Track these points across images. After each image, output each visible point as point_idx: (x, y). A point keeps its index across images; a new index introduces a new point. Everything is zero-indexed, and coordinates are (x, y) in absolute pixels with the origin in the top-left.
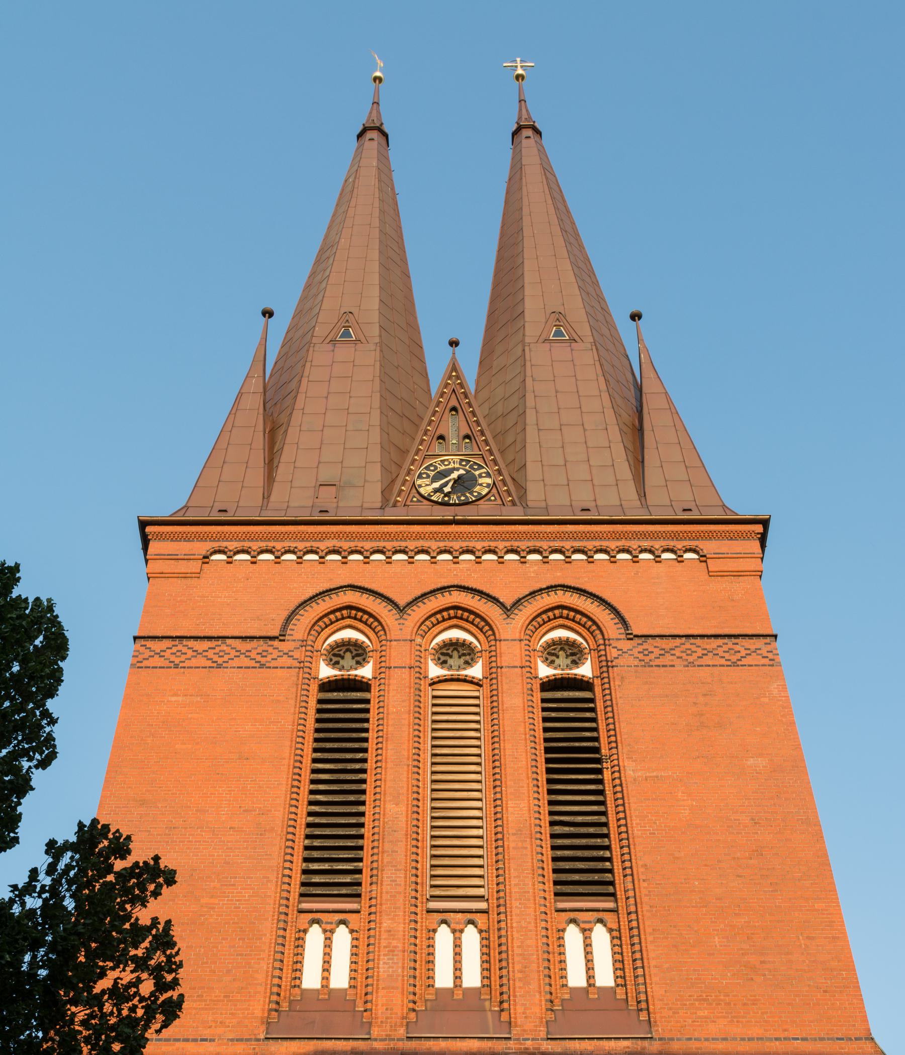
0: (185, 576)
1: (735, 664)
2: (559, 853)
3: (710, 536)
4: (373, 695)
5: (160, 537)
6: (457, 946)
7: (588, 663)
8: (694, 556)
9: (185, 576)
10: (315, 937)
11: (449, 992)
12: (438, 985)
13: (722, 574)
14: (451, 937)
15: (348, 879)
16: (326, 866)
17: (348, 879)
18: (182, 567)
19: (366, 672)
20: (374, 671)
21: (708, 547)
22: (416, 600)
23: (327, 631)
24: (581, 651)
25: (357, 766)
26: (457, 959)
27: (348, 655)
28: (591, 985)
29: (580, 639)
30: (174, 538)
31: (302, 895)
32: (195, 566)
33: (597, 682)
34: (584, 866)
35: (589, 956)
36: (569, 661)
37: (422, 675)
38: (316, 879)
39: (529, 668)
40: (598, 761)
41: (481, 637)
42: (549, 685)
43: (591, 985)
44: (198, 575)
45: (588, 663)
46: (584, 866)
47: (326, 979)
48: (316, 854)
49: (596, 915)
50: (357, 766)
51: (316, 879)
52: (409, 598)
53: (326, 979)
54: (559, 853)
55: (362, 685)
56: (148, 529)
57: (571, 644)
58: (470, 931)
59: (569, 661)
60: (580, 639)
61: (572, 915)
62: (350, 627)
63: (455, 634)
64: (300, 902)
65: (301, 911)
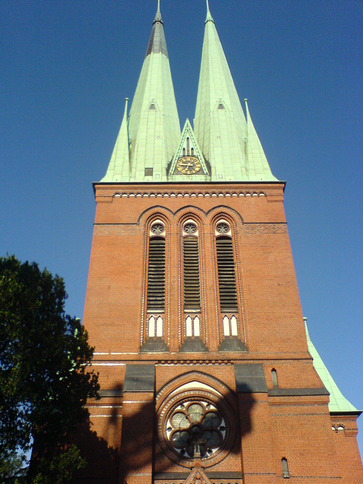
0: (107, 202)
1: (274, 233)
2: (222, 294)
3: (269, 188)
4: (233, 241)
5: (99, 188)
6: (193, 323)
7: (198, 232)
8: (263, 195)
9: (107, 202)
10: (226, 321)
11: (189, 337)
12: (195, 335)
13: (272, 201)
14: (228, 320)
15: (160, 303)
16: (154, 299)
17: (160, 303)
18: (107, 199)
19: (164, 234)
20: (166, 234)
21: (268, 192)
22: (178, 211)
23: (152, 221)
24: (195, 226)
25: (162, 266)
26: (193, 327)
27: (223, 227)
28: (156, 336)
29: (162, 222)
30: (103, 188)
31: (148, 308)
32: (110, 199)
33: (233, 238)
34: (228, 300)
35: (230, 326)
36: (192, 230)
37: (181, 236)
38: (151, 303)
39: (179, 234)
40: (233, 264)
41: (198, 222)
42: (219, 238)
43: (156, 336)
44: (111, 202)
45: (198, 232)
46: (228, 300)
47: (156, 334)
48: (151, 294)
49: (232, 314)
50: (162, 266)
51: (151, 303)
52: (208, 211)
53: (156, 334)
54: (222, 294)
55: (162, 239)
56: (96, 186)
57: (225, 224)
58: (234, 318)
59: (192, 230)
60: (162, 222)
61: (234, 314)
62: (222, 219)
63: (190, 221)
64: (184, 309)
65: (222, 312)
